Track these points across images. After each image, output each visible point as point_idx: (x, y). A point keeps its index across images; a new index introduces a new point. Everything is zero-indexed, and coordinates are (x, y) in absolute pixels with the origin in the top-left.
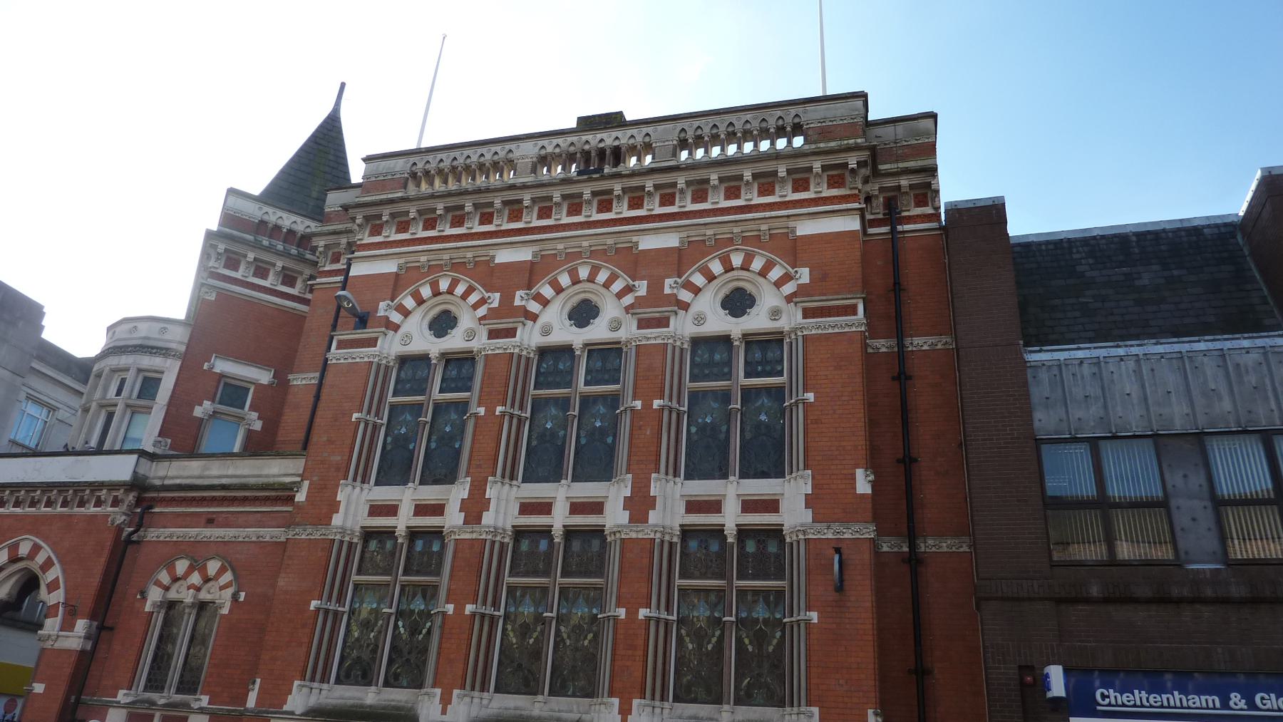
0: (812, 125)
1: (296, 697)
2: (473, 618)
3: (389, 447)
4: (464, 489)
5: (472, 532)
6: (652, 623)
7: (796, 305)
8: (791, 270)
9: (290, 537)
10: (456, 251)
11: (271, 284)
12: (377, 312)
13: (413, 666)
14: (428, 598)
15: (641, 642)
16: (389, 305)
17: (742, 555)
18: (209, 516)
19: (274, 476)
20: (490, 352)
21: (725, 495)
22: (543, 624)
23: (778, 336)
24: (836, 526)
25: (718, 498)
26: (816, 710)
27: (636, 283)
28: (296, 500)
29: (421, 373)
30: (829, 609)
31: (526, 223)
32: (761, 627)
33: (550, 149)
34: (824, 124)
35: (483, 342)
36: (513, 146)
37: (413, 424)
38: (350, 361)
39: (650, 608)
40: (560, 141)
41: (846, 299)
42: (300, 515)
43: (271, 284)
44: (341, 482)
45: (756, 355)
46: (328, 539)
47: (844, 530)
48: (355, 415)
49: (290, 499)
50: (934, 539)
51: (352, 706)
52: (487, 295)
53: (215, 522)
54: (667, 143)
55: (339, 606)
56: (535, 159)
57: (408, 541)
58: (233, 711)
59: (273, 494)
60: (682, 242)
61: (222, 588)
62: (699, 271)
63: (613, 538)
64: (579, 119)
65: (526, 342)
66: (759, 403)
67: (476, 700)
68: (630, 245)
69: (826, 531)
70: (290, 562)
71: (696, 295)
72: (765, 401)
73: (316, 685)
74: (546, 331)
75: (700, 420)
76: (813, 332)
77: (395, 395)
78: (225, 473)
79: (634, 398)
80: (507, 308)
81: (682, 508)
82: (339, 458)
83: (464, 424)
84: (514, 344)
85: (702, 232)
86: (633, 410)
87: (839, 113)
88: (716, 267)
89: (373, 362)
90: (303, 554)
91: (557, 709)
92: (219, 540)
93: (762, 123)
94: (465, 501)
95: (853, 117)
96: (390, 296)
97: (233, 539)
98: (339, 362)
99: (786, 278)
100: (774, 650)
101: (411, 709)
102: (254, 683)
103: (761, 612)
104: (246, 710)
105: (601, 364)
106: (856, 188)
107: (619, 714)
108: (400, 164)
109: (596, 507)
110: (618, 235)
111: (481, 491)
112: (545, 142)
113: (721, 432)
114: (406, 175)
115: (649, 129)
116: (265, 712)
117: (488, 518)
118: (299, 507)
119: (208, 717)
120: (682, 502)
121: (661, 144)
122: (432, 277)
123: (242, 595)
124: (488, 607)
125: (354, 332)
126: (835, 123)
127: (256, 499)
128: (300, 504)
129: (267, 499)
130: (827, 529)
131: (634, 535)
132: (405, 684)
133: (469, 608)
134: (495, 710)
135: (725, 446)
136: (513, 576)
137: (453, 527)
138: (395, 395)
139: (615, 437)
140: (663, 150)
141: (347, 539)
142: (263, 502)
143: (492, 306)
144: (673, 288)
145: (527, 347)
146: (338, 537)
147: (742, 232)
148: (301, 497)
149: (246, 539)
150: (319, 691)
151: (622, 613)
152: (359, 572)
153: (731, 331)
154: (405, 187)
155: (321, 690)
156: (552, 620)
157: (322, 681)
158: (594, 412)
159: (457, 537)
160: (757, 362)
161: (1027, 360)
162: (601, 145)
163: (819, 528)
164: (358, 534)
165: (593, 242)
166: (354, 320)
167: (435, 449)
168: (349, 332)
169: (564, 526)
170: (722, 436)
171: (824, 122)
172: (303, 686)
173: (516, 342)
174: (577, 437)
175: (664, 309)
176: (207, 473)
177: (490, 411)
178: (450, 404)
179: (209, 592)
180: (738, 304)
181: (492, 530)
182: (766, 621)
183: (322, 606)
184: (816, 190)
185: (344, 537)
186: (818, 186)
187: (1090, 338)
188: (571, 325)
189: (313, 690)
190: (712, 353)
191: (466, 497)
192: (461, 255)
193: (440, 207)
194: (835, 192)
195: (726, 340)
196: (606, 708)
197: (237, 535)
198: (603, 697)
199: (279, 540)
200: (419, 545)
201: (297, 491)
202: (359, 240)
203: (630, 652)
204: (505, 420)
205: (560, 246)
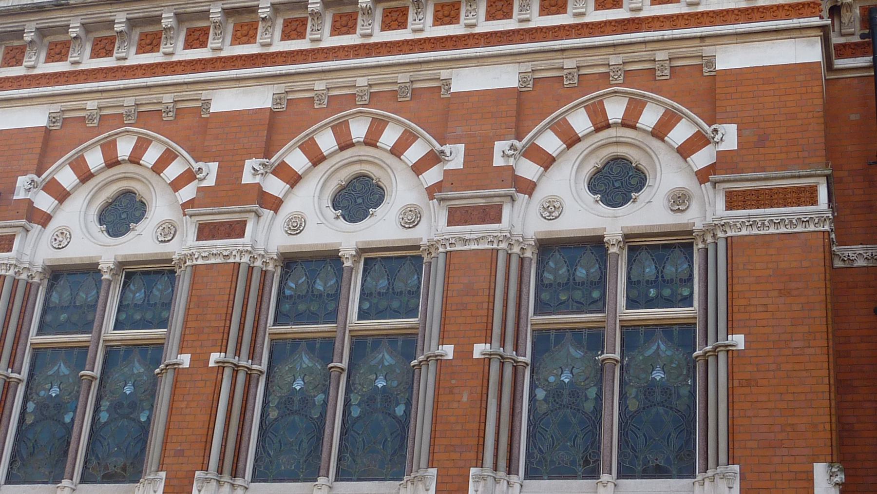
4: (155, 492)
8: (706, 127)
10: (146, 91)
16: (33, 181)
20: (200, 262)
23: (685, 239)
27: (447, 148)
35: (188, 245)
37: (71, 380)
41: (799, 177)
52: (196, 166)
60: (523, 80)
68: (199, 104)
74: (296, 227)
75: (42, 393)
76: (744, 232)
77: (41, 331)
83: (155, 382)
85: (557, 63)
110: (418, 67)
113: (587, 399)
122: (106, 134)
138: (41, 331)
143: (205, 184)
144: (508, 156)
145: (27, 266)
158: (373, 363)
170: (589, 406)
177: (200, 360)
184: (467, 22)
188: (337, 217)
190: (572, 265)
192: (154, 98)
204: (224, 376)
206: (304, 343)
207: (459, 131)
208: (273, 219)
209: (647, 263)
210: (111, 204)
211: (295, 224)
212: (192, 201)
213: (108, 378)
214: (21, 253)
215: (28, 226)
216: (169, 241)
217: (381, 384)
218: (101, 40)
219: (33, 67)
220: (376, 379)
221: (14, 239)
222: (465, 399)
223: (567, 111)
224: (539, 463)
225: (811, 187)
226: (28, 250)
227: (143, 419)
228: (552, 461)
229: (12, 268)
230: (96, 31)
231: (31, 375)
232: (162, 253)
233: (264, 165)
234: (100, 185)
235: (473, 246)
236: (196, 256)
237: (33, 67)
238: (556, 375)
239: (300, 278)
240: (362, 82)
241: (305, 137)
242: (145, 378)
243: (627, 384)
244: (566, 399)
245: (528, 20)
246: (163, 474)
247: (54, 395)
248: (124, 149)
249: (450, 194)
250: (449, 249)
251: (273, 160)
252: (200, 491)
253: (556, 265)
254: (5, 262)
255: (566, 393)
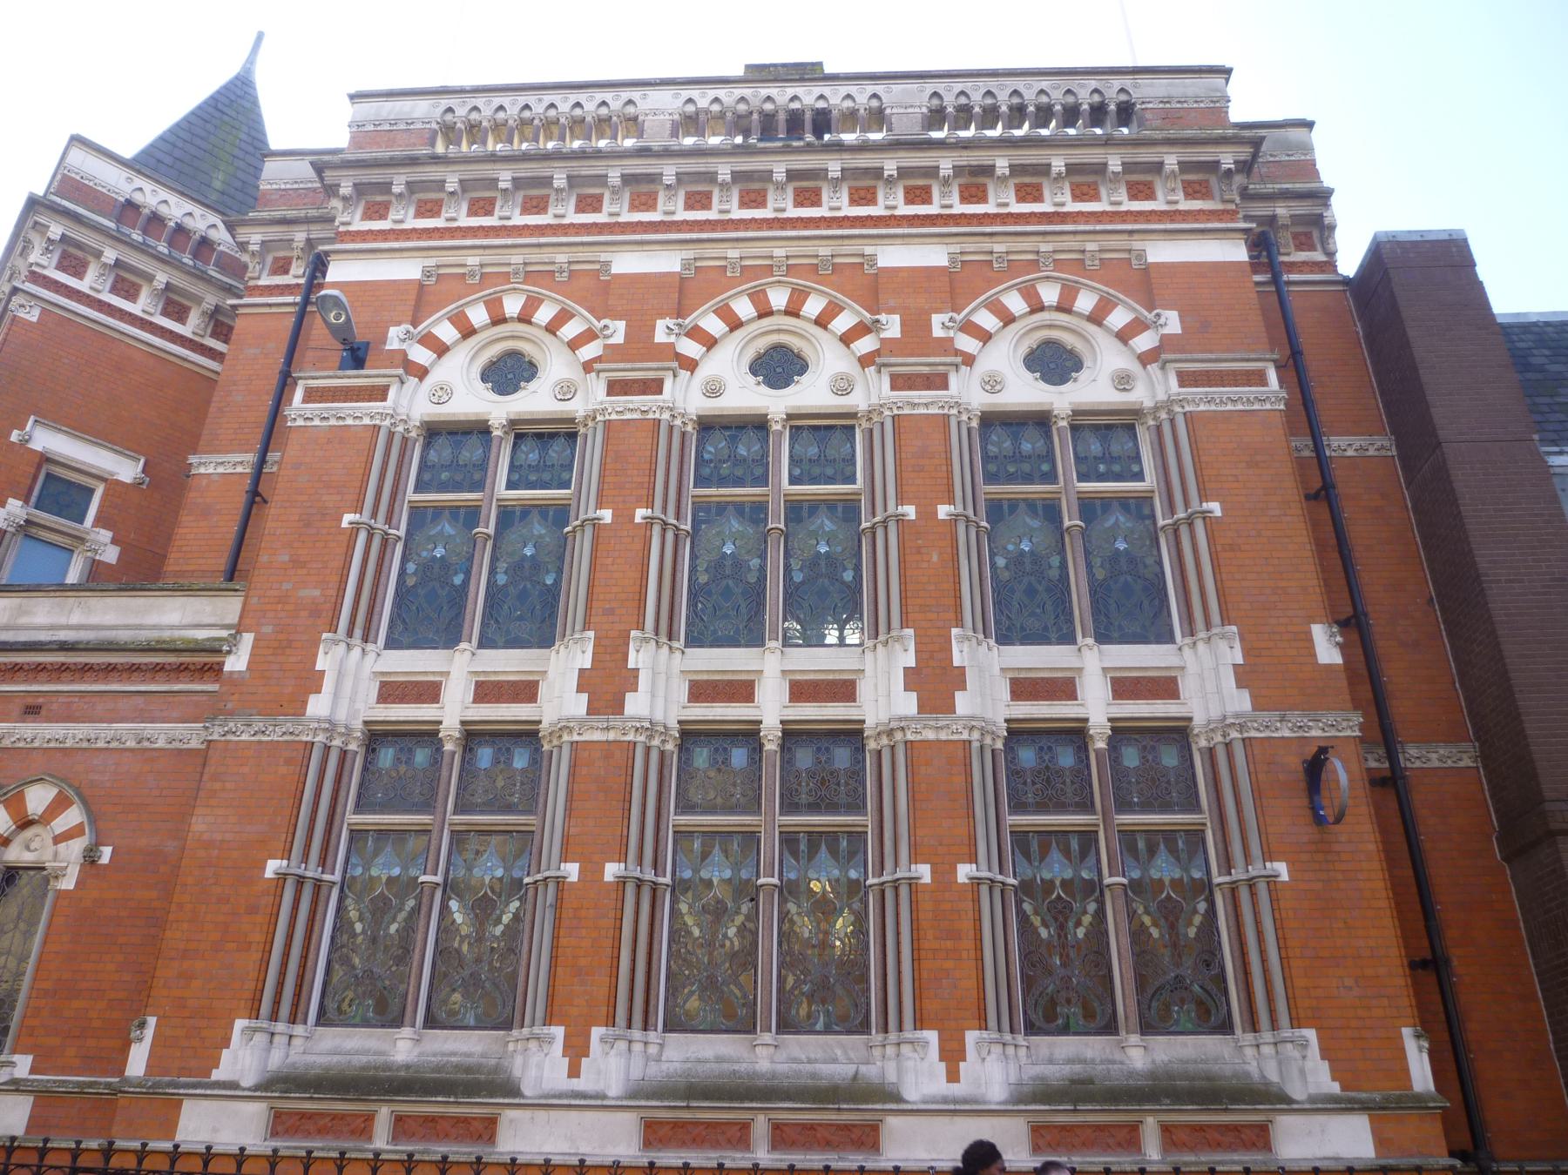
0: (1150, 106)
1: (241, 1053)
2: (621, 888)
3: (411, 582)
4: (583, 652)
5: (607, 729)
6: (984, 889)
7: (598, 376)
8: (1146, 313)
9: (215, 737)
10: (536, 250)
11: (91, 288)
12: (385, 343)
13: (487, 985)
14: (1183, 856)
15: (967, 925)
16: (408, 332)
17: (1119, 774)
18: (30, 701)
19: (172, 627)
20: (614, 417)
21: (1080, 670)
22: (752, 900)
23: (1127, 419)
24: (1296, 717)
25: (1068, 674)
26: (1311, 1034)
27: (883, 317)
28: (227, 668)
29: (468, 455)
30: (1304, 857)
31: (395, 222)
32: (486, 892)
33: (703, 103)
34: (1168, 106)
35: (599, 399)
36: (635, 94)
37: (458, 540)
38: (333, 422)
39: (289, 859)
40: (721, 93)
41: (1248, 360)
42: (236, 696)
43: (91, 288)
44: (325, 635)
45: (1093, 447)
46: (302, 742)
47: (1310, 724)
48: (348, 519)
49: (215, 670)
50: (1418, 748)
51: (363, 1068)
52: (598, 325)
53: (43, 712)
54: (910, 110)
55: (322, 873)
56: (676, 117)
57: (461, 748)
58: (91, 1085)
59: (171, 659)
60: (952, 261)
61: (58, 840)
62: (986, 307)
63: (885, 741)
64: (747, 67)
65: (680, 404)
66: (1112, 521)
67: (638, 1047)
68: (597, 267)
69: (1278, 725)
70: (217, 786)
71: (440, 356)
72: (1118, 518)
73: (280, 1027)
74: (714, 390)
75: (424, 554)
76: (1202, 407)
77: (417, 489)
78: (63, 621)
79: (600, 505)
80: (640, 345)
81: (1005, 694)
82: (317, 593)
83: (563, 543)
84: (661, 404)
85: (987, 246)
86: (595, 523)
87: (1190, 92)
88: (744, 308)
89: (380, 427)
90: (246, 770)
91: (803, 1057)
92: (52, 745)
93: (628, 107)
94: (587, 672)
95: (1215, 99)
96: (410, 318)
97: (85, 745)
98: (309, 423)
99: (861, 330)
100: (503, 933)
101: (497, 1069)
102: (142, 1025)
103: (1164, 869)
104: (127, 1081)
105: (816, 450)
106: (1232, 201)
107: (941, 1060)
108: (421, 109)
109: (526, 691)
110: (840, 242)
111: (619, 656)
112: (694, 93)
113: (1050, 567)
114: (434, 126)
115: (879, 88)
116: (169, 1085)
117: (636, 705)
118: (235, 680)
119: (31, 1099)
120: (783, 682)
121: (902, 111)
122: (491, 291)
123: (106, 854)
124: (294, 863)
125: (340, 373)
126: (1185, 105)
127: (133, 669)
128: (236, 676)
129: (159, 669)
130: (1281, 721)
131: (930, 735)
132: (472, 1023)
133: (612, 870)
134: (677, 1065)
135: (459, 597)
136: (683, 813)
137: (568, 720)
138: (417, 489)
139: (560, 571)
140: (905, 120)
141: (337, 742)
142: (54, 675)
143: (611, 341)
144: (948, 328)
145: (405, 417)
146: (321, 738)
147: (1054, 252)
148: (236, 663)
149: (114, 745)
150: (285, 1039)
151: (924, 872)
152: (359, 808)
153: (1052, 404)
154: (433, 145)
155: (291, 1036)
156: (332, 887)
157: (293, 1020)
159: (576, 738)
160: (1095, 458)
161: (1550, 464)
162: (795, 105)
163: (1267, 720)
164: (359, 734)
165: (794, 249)
166: (337, 353)
167: (803, 583)
168: (331, 373)
169: (463, 723)
170: (1054, 573)
171: (1168, 102)
172: (255, 1030)
173: (664, 401)
174: (399, 575)
175: (938, 360)
176: (23, 620)
177: (622, 516)
178: (527, 510)
179: (28, 848)
180: (509, 377)
181: (647, 725)
182: (1176, 884)
183: (292, 871)
184: (776, 206)
185: (331, 739)
186: (667, 204)
187: (1553, 441)
188: (759, 383)
189: (277, 1039)
190: (1016, 439)
191: (588, 665)
192: (545, 258)
193: (505, 177)
194: (1197, 205)
195: (480, 429)
196: (916, 1051)
197: (93, 736)
198: (900, 1029)
199: (185, 746)
200: (485, 755)
201: (229, 652)
202: (343, 224)
203: (949, 944)
204: (653, 533)
205: (733, 253)
206: (730, 508)
207: (892, 303)
208: (689, 380)
209: (1092, 440)
210: (494, 363)
211: (713, 387)
212: (600, 357)
213: (504, 538)
214: (396, 402)
215: (404, 377)
216: (569, 399)
217: (823, 549)
218: (478, 200)
219: (401, 221)
220: (818, 544)
221: (388, 389)
222: (935, 558)
223: (1000, 292)
224: (1009, 629)
225: (1260, 371)
226: (404, 402)
227: (549, 581)
228: (1022, 627)
229: (388, 418)
230: (583, 186)
231: (408, 532)
232: (562, 411)
233: (679, 325)
234: (482, 344)
235: (922, 411)
236: (610, 411)
237: (401, 221)
238: (1015, 544)
239: (720, 443)
240: (779, 252)
241: (719, 302)
242: (548, 539)
243: (1090, 553)
244: (1028, 567)
245: (728, 212)
246: (591, 634)
247: (438, 556)
248: (512, 306)
249: (893, 360)
250: (896, 412)
251: (687, 321)
252: (638, 651)
253: (999, 438)
254: (381, 411)
255: (1027, 561)
